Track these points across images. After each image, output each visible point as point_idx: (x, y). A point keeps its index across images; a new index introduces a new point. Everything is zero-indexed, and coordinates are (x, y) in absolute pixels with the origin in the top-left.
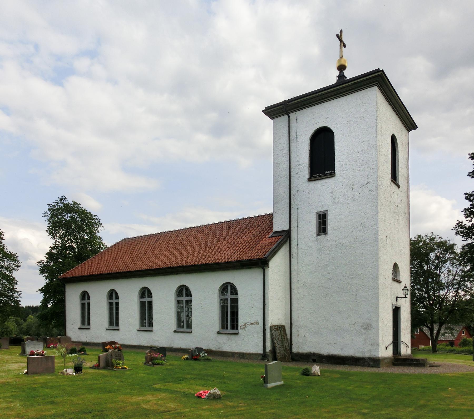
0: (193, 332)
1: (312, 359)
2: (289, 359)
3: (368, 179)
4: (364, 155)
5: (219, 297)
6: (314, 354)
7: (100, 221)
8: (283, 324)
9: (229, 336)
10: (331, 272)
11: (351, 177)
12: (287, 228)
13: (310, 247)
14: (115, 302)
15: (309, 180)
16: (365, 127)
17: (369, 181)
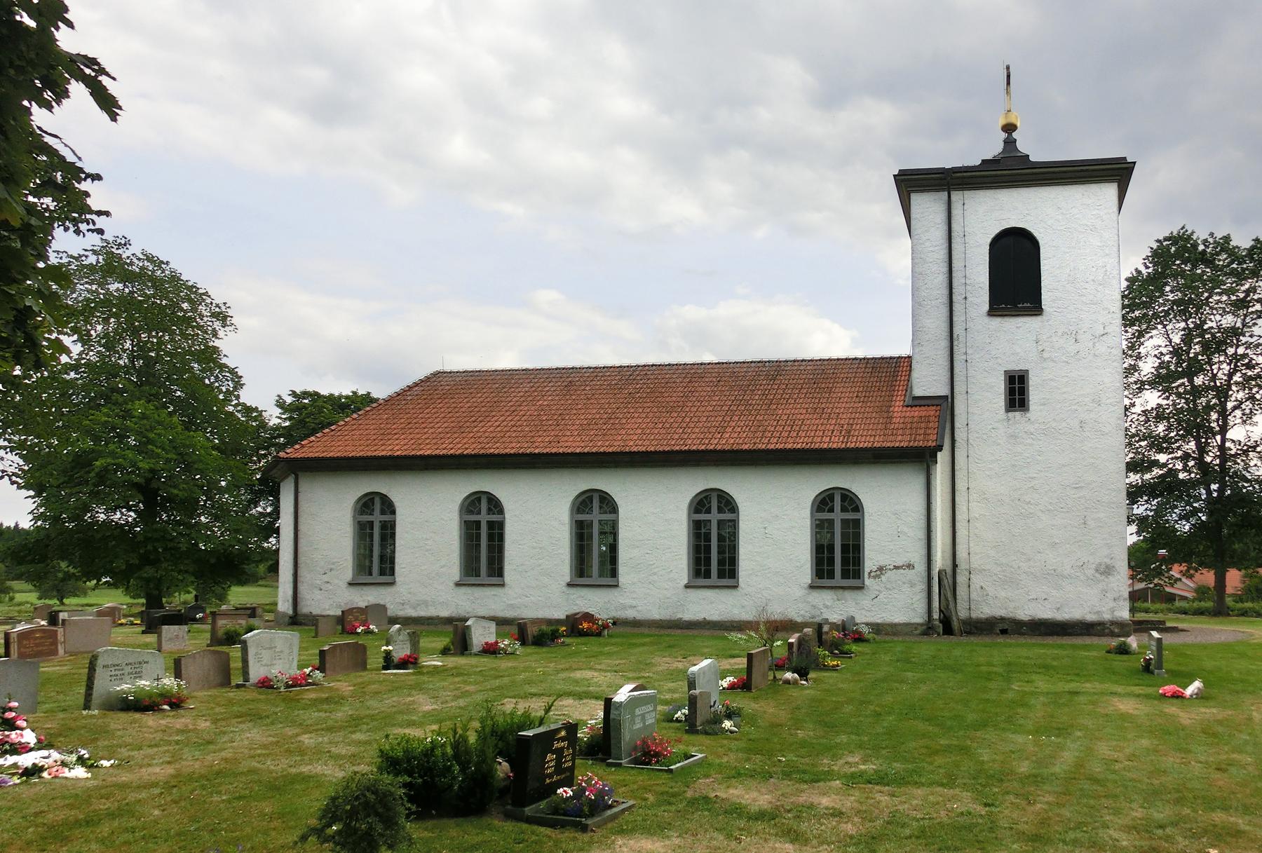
5: (461, 517)
6: (1002, 619)
7: (228, 310)
9: (840, 592)
10: (1035, 475)
12: (943, 390)
14: (488, 522)
16: (1099, 244)
17: (1106, 331)
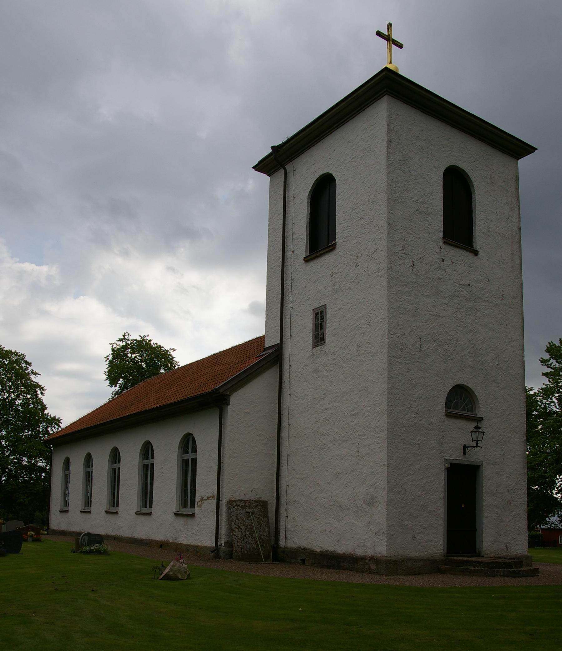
0: (153, 513)
1: (301, 558)
2: (267, 557)
3: (375, 244)
4: (370, 207)
8: (264, 498)
11: (355, 245)
13: (304, 368)
15: (307, 260)
